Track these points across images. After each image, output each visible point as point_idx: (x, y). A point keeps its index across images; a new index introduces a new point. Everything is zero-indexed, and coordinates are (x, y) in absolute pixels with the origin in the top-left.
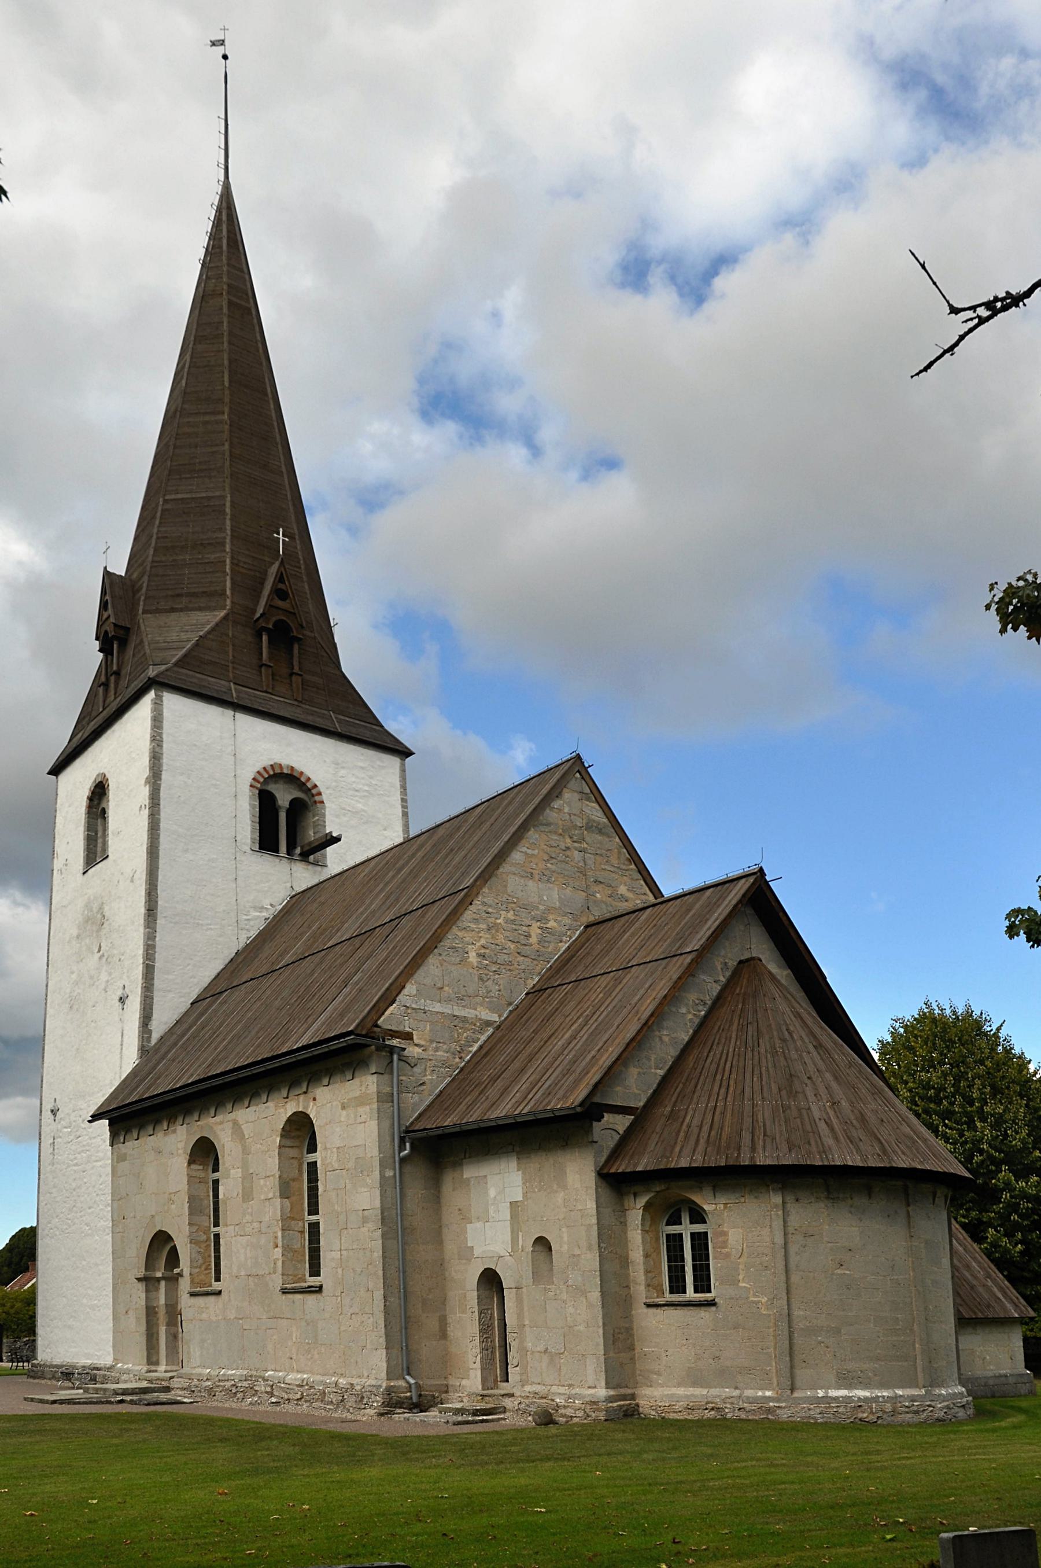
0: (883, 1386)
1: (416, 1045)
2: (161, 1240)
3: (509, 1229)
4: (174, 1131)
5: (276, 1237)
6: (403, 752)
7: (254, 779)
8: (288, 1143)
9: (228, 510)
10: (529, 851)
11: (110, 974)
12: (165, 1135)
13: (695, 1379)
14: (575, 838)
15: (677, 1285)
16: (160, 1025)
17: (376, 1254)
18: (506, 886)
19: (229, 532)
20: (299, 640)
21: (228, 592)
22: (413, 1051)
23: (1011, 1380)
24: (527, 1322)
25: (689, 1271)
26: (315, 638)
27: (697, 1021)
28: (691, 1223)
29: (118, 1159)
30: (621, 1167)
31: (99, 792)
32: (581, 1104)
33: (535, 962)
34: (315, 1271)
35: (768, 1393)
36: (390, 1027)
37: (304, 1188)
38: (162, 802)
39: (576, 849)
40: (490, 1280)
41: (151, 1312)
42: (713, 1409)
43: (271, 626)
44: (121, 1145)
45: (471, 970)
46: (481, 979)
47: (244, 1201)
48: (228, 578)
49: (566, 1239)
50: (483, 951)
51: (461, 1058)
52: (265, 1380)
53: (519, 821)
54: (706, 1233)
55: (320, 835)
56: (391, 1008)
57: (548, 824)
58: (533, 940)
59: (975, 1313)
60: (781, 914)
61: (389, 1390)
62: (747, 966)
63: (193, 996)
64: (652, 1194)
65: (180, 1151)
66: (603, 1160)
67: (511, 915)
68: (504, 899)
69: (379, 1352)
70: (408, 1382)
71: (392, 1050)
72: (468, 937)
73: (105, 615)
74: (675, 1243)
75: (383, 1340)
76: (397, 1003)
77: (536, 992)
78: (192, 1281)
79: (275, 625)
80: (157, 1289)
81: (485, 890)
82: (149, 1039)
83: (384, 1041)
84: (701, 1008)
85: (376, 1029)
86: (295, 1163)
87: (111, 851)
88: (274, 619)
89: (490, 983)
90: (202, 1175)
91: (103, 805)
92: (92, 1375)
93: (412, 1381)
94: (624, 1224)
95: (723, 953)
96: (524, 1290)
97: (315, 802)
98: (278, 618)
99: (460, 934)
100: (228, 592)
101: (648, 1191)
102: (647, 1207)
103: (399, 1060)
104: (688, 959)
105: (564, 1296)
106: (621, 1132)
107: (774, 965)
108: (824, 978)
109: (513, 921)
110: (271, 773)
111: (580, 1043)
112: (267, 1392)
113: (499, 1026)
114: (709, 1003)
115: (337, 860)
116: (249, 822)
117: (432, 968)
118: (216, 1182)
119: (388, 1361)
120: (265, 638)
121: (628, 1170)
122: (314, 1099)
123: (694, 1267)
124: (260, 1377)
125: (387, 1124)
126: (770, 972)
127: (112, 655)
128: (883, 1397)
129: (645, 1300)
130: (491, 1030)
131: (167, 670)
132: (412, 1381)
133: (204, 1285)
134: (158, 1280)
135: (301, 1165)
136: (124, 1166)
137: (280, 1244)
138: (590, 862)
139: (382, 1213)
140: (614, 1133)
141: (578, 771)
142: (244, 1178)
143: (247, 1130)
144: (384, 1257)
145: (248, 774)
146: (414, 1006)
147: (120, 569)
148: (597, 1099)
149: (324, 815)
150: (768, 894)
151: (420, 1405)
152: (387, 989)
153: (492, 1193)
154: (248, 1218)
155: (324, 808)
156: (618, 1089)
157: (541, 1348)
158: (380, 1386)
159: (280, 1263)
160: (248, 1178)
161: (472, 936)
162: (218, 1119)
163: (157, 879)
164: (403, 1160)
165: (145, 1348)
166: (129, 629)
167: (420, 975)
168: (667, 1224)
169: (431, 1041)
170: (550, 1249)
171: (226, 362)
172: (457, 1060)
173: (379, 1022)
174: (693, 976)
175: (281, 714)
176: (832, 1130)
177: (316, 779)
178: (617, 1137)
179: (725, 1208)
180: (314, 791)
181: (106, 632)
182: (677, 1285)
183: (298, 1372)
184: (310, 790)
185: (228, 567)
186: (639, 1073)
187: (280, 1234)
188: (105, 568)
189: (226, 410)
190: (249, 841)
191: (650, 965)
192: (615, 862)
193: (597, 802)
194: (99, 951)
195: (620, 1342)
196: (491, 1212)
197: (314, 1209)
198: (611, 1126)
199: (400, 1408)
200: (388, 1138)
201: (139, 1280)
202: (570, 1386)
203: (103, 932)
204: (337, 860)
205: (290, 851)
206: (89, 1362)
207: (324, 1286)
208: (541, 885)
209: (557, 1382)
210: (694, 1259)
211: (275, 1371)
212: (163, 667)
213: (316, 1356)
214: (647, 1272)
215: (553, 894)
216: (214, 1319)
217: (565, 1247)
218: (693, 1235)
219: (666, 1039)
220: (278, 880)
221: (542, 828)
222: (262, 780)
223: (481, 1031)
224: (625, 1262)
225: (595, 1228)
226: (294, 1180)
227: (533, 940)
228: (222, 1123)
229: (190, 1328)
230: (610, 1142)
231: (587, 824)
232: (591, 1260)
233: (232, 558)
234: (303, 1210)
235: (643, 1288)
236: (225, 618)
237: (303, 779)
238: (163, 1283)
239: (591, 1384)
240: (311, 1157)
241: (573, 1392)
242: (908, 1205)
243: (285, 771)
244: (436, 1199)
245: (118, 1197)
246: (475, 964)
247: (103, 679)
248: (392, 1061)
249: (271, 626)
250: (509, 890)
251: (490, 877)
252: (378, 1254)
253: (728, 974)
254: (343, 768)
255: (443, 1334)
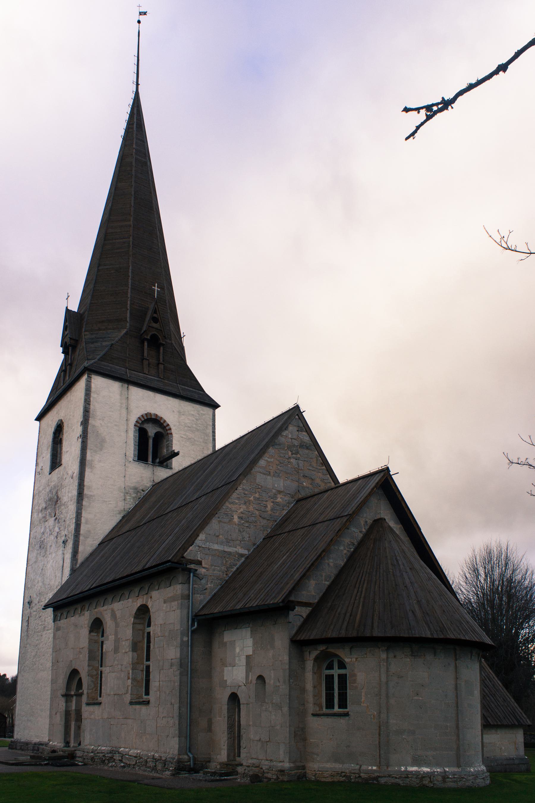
0: (438, 765)
1: (204, 568)
2: (74, 673)
3: (245, 671)
4: (84, 615)
5: (129, 674)
6: (214, 406)
7: (136, 422)
8: (137, 621)
9: (130, 274)
10: (269, 460)
11: (59, 528)
12: (80, 616)
13: (336, 758)
14: (294, 452)
15: (330, 704)
16: (81, 558)
17: (176, 684)
18: (255, 479)
19: (130, 286)
20: (163, 345)
21: (128, 320)
22: (202, 571)
23: (516, 762)
24: (251, 723)
25: (337, 696)
26: (172, 343)
27: (349, 554)
28: (339, 668)
29: (57, 629)
30: (303, 637)
31: (59, 429)
32: (283, 601)
33: (269, 521)
34: (147, 693)
35: (374, 768)
36: (190, 558)
37: (143, 646)
38: (89, 435)
39: (294, 458)
40: (234, 698)
41: (67, 713)
42: (344, 776)
43: (149, 338)
44: (58, 622)
45: (234, 526)
46: (240, 531)
47: (115, 653)
48: (128, 311)
49: (273, 677)
50: (242, 515)
51: (226, 575)
52: (119, 753)
53: (264, 443)
54: (346, 675)
55: (170, 451)
56: (191, 548)
57: (279, 445)
58: (269, 508)
59: (497, 722)
60: (397, 493)
61: (179, 761)
62: (379, 522)
63: (100, 540)
64: (319, 652)
65: (86, 626)
66: (294, 632)
67: (257, 495)
68: (254, 486)
69: (175, 739)
70: (188, 756)
71: (190, 570)
72: (234, 507)
73: (66, 333)
74: (329, 679)
75: (177, 732)
76: (194, 544)
77: (268, 538)
78: (88, 697)
79: (151, 336)
80: (71, 702)
81: (244, 481)
82: (76, 563)
83: (186, 566)
84: (351, 547)
85: (182, 559)
86: (141, 632)
87: (64, 461)
88: (151, 334)
89: (244, 533)
90: (96, 638)
91: (61, 437)
92: (37, 746)
93: (191, 756)
94: (304, 669)
95: (365, 515)
96: (251, 705)
97: (168, 434)
98: (153, 333)
99: (229, 506)
100: (128, 320)
101: (316, 650)
102: (316, 659)
103: (194, 576)
104: (345, 519)
105: (270, 709)
106: (305, 617)
107: (393, 523)
108: (420, 529)
109: (259, 498)
110: (146, 418)
111: (286, 567)
112: (120, 760)
113: (248, 557)
114: (356, 544)
115: (178, 464)
116: (133, 445)
117: (214, 525)
118: (102, 642)
119: (179, 744)
120: (146, 344)
121: (306, 638)
122: (151, 597)
123: (339, 693)
124: (117, 751)
125: (185, 611)
126: (389, 526)
127: (68, 355)
128: (438, 772)
129: (312, 712)
130: (243, 559)
131: (95, 363)
132: (191, 756)
133: (93, 699)
134: (72, 696)
135: (144, 633)
136: (59, 633)
137: (131, 677)
138: (301, 465)
139: (181, 661)
140: (301, 618)
141: (297, 415)
142: (115, 641)
143: (118, 614)
144: (180, 686)
145: (133, 419)
146: (203, 546)
147: (75, 308)
148: (292, 598)
149: (172, 441)
150: (391, 481)
151: (194, 770)
152: (190, 537)
153: (237, 650)
154: (116, 662)
155: (172, 437)
156: (304, 592)
157: (257, 738)
158: (174, 758)
159: (130, 688)
160: (117, 641)
161: (236, 507)
162: (105, 607)
163: (84, 477)
164: (193, 632)
165: (63, 733)
166: (77, 340)
167: (207, 529)
168: (327, 669)
169: (212, 565)
170: (265, 683)
171: (133, 193)
172: (225, 576)
173: (185, 555)
174: (348, 529)
175: (152, 386)
176: (415, 616)
177: (169, 421)
178: (302, 620)
179: (356, 660)
180: (167, 428)
181: (66, 342)
182: (330, 704)
183: (136, 749)
184: (165, 427)
185: (128, 305)
186: (316, 583)
187: (131, 671)
188: (67, 307)
189: (132, 219)
190: (132, 456)
191: (326, 523)
192: (315, 465)
193: (306, 431)
194: (55, 516)
195: (300, 735)
196: (237, 661)
197: (148, 659)
198: (299, 613)
199: (184, 771)
200: (186, 620)
201: (63, 696)
202: (271, 760)
203: (58, 505)
204: (178, 464)
205: (153, 461)
206: (38, 740)
207: (151, 701)
208: (274, 478)
209: (265, 758)
210: (339, 689)
211: (125, 748)
212: (93, 361)
213: (145, 740)
214: (314, 696)
215: (280, 484)
216: (97, 718)
217: (272, 681)
218: (339, 675)
219: (331, 564)
220: (144, 476)
221: (276, 447)
222: (140, 422)
223: (238, 560)
224: (303, 690)
225: (288, 671)
226: (140, 642)
227: (269, 508)
228: (106, 610)
229: (86, 724)
230: (298, 622)
231: (300, 444)
232: (284, 689)
233: (131, 301)
234: (143, 658)
235: (311, 705)
236: (126, 334)
237: (162, 421)
238: (75, 698)
239: (281, 759)
240: (148, 630)
241: (272, 764)
242: (456, 660)
243: (153, 417)
244: (209, 653)
245: (56, 650)
246: (237, 523)
247: (64, 368)
248: (190, 577)
249: (149, 338)
250: (257, 481)
251: (247, 474)
252: (177, 684)
253: (367, 527)
254: (183, 415)
255: (209, 729)
